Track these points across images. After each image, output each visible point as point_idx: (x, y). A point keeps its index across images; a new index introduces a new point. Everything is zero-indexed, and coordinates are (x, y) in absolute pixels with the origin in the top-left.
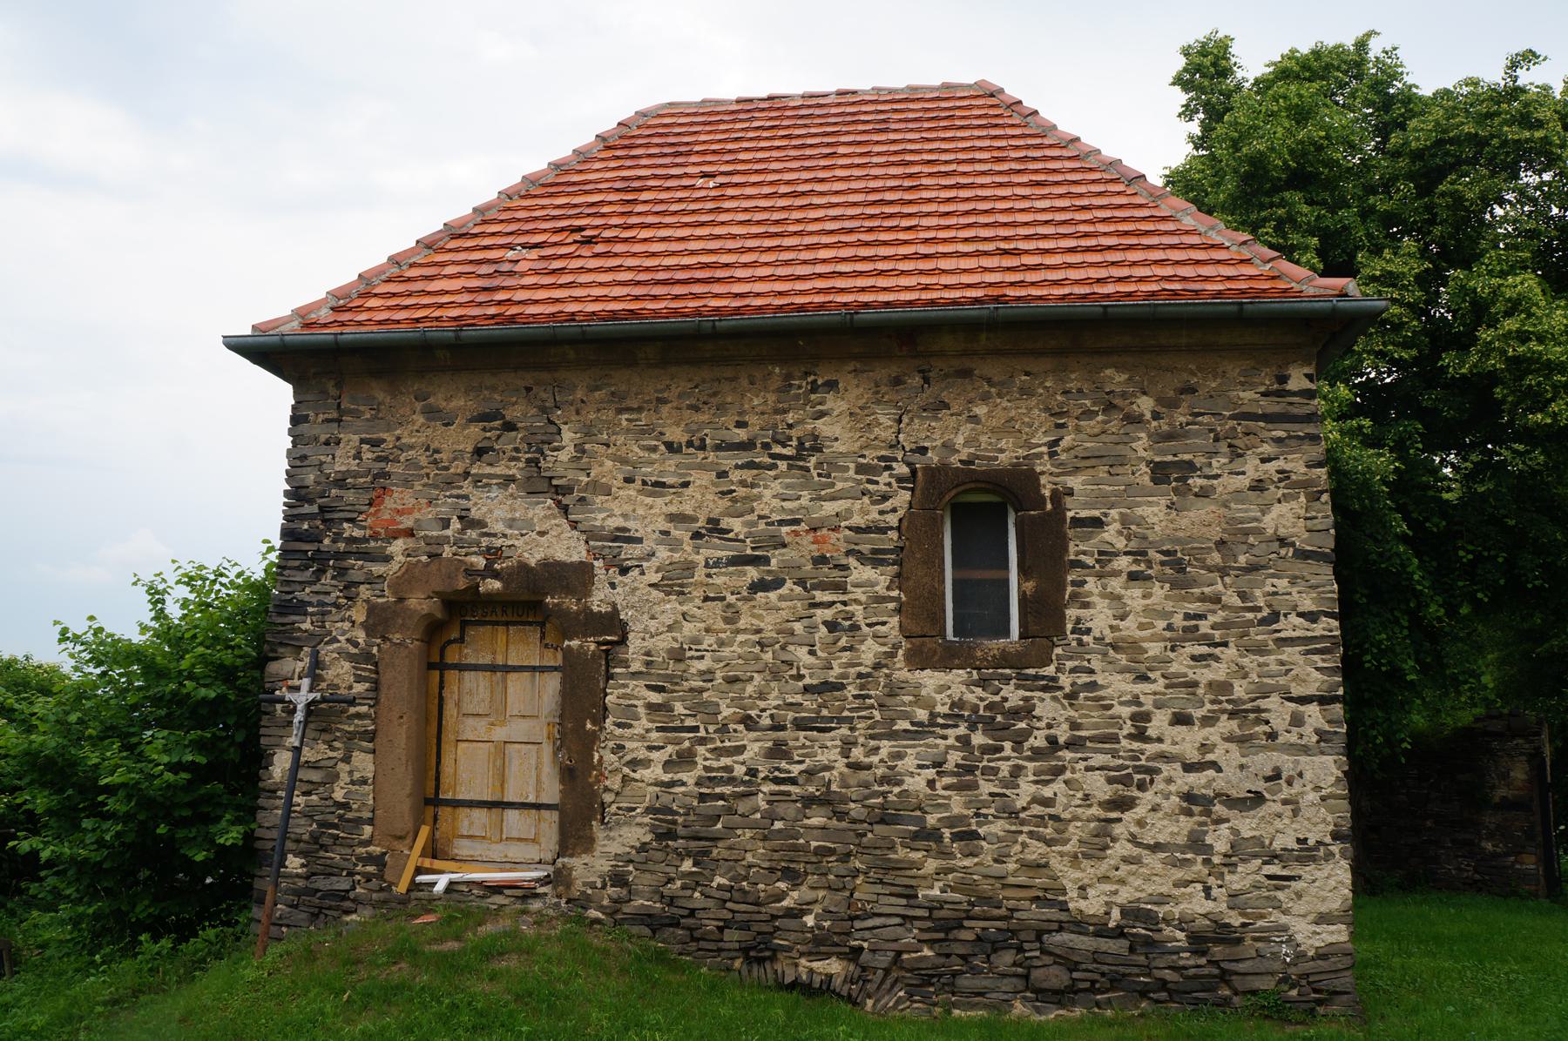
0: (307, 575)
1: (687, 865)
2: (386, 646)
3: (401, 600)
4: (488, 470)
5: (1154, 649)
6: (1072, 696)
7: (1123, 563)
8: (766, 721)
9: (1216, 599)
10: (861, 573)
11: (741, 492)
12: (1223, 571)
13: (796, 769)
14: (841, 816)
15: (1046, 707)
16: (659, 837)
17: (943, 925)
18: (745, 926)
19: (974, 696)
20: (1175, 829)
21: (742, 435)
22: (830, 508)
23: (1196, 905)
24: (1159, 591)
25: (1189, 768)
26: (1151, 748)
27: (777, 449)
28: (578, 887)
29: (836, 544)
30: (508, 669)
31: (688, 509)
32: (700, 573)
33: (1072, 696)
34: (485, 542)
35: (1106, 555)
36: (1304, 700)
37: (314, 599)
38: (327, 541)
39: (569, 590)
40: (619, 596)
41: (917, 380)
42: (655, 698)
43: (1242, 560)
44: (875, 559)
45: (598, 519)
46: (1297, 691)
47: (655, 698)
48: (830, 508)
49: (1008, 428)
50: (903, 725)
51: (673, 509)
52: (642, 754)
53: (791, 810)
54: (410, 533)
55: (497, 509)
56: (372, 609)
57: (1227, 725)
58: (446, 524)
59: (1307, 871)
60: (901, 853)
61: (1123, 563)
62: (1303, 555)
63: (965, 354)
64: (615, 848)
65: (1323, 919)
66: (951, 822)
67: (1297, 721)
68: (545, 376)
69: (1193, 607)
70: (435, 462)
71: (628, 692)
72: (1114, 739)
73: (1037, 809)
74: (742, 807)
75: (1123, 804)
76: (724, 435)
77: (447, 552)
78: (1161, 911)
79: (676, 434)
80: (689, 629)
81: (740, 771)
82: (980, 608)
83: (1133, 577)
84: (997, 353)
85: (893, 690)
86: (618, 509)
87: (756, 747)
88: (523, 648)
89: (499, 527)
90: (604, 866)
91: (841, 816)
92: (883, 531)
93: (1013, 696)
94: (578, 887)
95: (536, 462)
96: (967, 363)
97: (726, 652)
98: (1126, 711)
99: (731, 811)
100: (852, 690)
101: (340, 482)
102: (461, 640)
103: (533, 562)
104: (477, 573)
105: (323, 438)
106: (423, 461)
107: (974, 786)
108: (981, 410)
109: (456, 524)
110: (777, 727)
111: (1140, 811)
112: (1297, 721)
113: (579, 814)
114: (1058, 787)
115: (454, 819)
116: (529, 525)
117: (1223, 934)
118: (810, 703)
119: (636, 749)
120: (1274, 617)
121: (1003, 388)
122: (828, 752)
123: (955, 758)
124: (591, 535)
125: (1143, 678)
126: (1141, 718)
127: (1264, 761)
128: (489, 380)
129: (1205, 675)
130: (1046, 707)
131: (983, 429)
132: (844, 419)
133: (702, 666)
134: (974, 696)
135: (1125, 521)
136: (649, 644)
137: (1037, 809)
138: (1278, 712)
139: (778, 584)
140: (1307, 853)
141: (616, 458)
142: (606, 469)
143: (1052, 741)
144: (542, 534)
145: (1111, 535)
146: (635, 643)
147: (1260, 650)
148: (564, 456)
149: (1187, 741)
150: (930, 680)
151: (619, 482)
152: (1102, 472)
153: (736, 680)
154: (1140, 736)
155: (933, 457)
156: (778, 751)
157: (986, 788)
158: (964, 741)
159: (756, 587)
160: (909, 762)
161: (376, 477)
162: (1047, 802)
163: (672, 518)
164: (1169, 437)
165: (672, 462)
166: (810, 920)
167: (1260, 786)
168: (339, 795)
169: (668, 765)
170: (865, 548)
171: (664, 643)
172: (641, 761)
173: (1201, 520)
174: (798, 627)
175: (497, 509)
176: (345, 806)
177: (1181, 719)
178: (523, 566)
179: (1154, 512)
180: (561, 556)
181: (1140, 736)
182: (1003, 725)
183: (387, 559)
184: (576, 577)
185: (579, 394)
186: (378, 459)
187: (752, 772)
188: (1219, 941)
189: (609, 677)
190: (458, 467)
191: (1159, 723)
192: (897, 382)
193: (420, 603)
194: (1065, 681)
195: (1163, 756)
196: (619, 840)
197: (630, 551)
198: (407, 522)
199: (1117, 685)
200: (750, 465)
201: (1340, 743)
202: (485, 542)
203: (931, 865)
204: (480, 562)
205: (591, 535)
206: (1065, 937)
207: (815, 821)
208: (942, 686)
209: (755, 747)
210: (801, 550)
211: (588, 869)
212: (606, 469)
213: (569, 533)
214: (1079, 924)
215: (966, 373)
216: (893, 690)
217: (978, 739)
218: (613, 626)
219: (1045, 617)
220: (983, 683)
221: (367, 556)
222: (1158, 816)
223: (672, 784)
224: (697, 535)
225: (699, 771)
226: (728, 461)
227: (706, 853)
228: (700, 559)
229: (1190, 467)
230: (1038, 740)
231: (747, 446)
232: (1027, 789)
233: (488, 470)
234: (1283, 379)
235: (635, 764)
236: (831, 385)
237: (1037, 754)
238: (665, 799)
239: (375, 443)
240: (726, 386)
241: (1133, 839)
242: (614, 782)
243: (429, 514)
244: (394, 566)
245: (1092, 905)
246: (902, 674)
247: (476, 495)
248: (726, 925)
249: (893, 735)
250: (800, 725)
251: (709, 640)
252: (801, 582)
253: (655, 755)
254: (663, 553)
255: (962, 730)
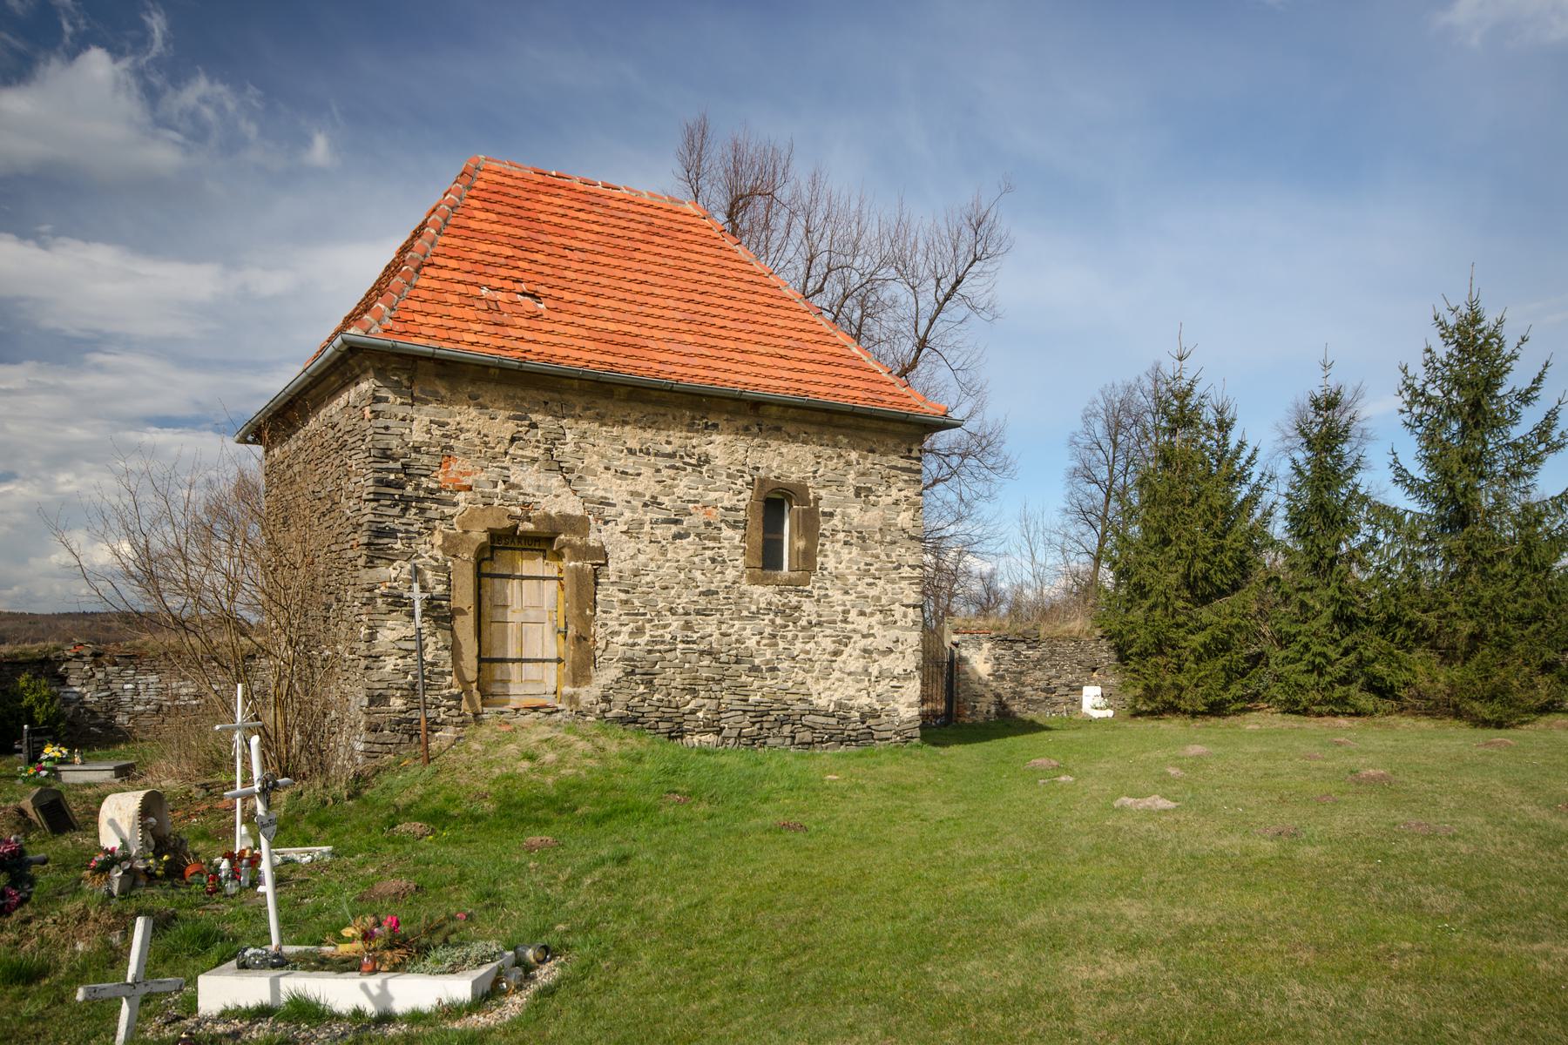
0: (397, 511)
1: (642, 689)
2: (458, 561)
3: (466, 532)
4: (520, 452)
5: (852, 579)
6: (818, 601)
7: (841, 536)
8: (681, 611)
9: (878, 557)
10: (727, 532)
11: (669, 482)
12: (881, 543)
13: (695, 636)
14: (717, 660)
15: (808, 606)
16: (627, 674)
17: (760, 715)
18: (670, 720)
19: (776, 599)
20: (855, 665)
21: (669, 449)
22: (712, 496)
23: (863, 700)
24: (855, 551)
25: (864, 636)
26: (849, 627)
27: (687, 460)
28: (583, 704)
29: (716, 516)
30: (544, 578)
31: (640, 489)
32: (647, 528)
33: (818, 601)
34: (521, 498)
35: (834, 531)
36: (908, 606)
37: (403, 528)
38: (409, 488)
39: (575, 532)
40: (604, 537)
41: (756, 429)
42: (623, 596)
43: (888, 538)
44: (734, 525)
45: (590, 491)
46: (906, 602)
47: (623, 596)
48: (712, 496)
49: (795, 461)
50: (745, 613)
51: (631, 488)
52: (617, 628)
53: (694, 657)
54: (470, 489)
55: (528, 478)
56: (446, 537)
57: (879, 616)
58: (495, 485)
59: (906, 684)
60: (744, 678)
61: (841, 536)
62: (912, 538)
63: (780, 418)
64: (603, 681)
65: (910, 705)
66: (768, 662)
67: (905, 616)
68: (556, 396)
69: (869, 560)
70: (486, 443)
71: (608, 592)
72: (834, 622)
73: (802, 656)
74: (669, 656)
75: (836, 653)
76: (658, 447)
77: (497, 502)
78: (850, 703)
79: (633, 444)
80: (642, 558)
81: (668, 637)
82: (769, 557)
83: (846, 543)
84: (794, 420)
85: (742, 595)
86: (601, 485)
87: (675, 624)
88: (532, 566)
89: (529, 490)
90: (597, 692)
91: (717, 660)
92: (737, 510)
93: (794, 599)
94: (583, 704)
95: (550, 450)
96: (780, 423)
97: (661, 572)
98: (840, 609)
99: (663, 659)
100: (721, 595)
101: (417, 449)
102: (492, 559)
103: (553, 513)
104: (519, 518)
105: (400, 416)
106: (477, 441)
107: (776, 645)
108: (784, 450)
109: (501, 486)
110: (687, 614)
111: (844, 656)
112: (905, 616)
113: (582, 665)
114: (811, 645)
115: (491, 671)
116: (549, 490)
117: (875, 714)
118: (703, 601)
119: (614, 625)
120: (898, 567)
121: (795, 439)
122: (710, 627)
123: (768, 630)
124: (585, 499)
125: (846, 593)
126: (846, 612)
127: (894, 633)
128: (520, 393)
129: (872, 592)
130: (808, 606)
131: (788, 460)
132: (722, 447)
133: (648, 579)
134: (776, 599)
135: (844, 515)
136: (621, 565)
137: (802, 656)
138: (898, 610)
139: (687, 535)
140: (907, 675)
141: (598, 453)
142: (592, 460)
143: (810, 623)
144: (557, 496)
145: (836, 521)
146: (612, 566)
147: (893, 582)
148: (568, 449)
149: (862, 624)
150: (758, 590)
151: (601, 469)
152: (834, 489)
153: (666, 588)
154: (845, 621)
155: (762, 473)
156: (688, 626)
157: (781, 645)
158: (773, 622)
159: (675, 537)
160: (748, 632)
161: (443, 448)
162: (808, 652)
163: (632, 494)
164: (863, 474)
165: (632, 459)
166: (700, 714)
167: (891, 645)
168: (428, 658)
169: (631, 634)
170: (730, 519)
171: (628, 566)
172: (616, 634)
173: (873, 517)
174: (696, 559)
175: (528, 478)
176: (433, 664)
177: (862, 613)
178: (548, 516)
179: (854, 511)
180: (569, 511)
181: (845, 621)
182: (789, 613)
183: (455, 505)
184: (578, 525)
185: (578, 411)
186: (444, 436)
187: (674, 638)
188: (873, 717)
189: (597, 584)
190: (500, 449)
191: (853, 616)
192: (747, 429)
193: (479, 536)
194: (815, 593)
195: (854, 631)
196: (607, 675)
197: (609, 511)
198: (468, 481)
199: (836, 596)
200: (672, 467)
201: (920, 627)
202: (521, 498)
203: (756, 684)
204: (518, 511)
205: (585, 499)
206: (811, 717)
207: (705, 663)
208: (763, 594)
209: (675, 624)
210: (699, 518)
211: (589, 694)
212: (592, 460)
213: (572, 498)
214: (815, 712)
215: (778, 429)
216: (742, 595)
217: (779, 621)
218: (600, 555)
219: (807, 561)
220: (781, 593)
221: (439, 501)
222: (851, 659)
223: (634, 645)
224: (645, 505)
225: (647, 638)
226: (662, 463)
227: (651, 682)
228: (647, 518)
229: (870, 489)
230: (803, 622)
231: (672, 456)
232: (799, 645)
233: (520, 452)
234: (910, 451)
235: (613, 633)
236: (715, 426)
237: (804, 628)
238: (629, 654)
239: (442, 425)
240: (661, 419)
241: (841, 670)
242: (601, 644)
243: (483, 477)
244: (460, 509)
245: (822, 702)
246: (745, 586)
247: (514, 468)
248: (662, 719)
249: (741, 618)
250: (698, 613)
251: (652, 565)
252: (698, 535)
253: (624, 629)
254: (628, 515)
255: (771, 616)
